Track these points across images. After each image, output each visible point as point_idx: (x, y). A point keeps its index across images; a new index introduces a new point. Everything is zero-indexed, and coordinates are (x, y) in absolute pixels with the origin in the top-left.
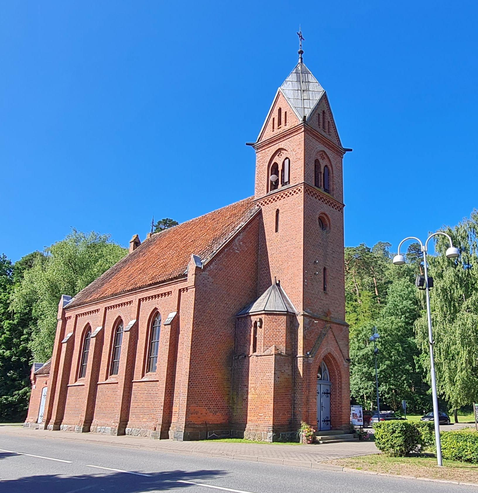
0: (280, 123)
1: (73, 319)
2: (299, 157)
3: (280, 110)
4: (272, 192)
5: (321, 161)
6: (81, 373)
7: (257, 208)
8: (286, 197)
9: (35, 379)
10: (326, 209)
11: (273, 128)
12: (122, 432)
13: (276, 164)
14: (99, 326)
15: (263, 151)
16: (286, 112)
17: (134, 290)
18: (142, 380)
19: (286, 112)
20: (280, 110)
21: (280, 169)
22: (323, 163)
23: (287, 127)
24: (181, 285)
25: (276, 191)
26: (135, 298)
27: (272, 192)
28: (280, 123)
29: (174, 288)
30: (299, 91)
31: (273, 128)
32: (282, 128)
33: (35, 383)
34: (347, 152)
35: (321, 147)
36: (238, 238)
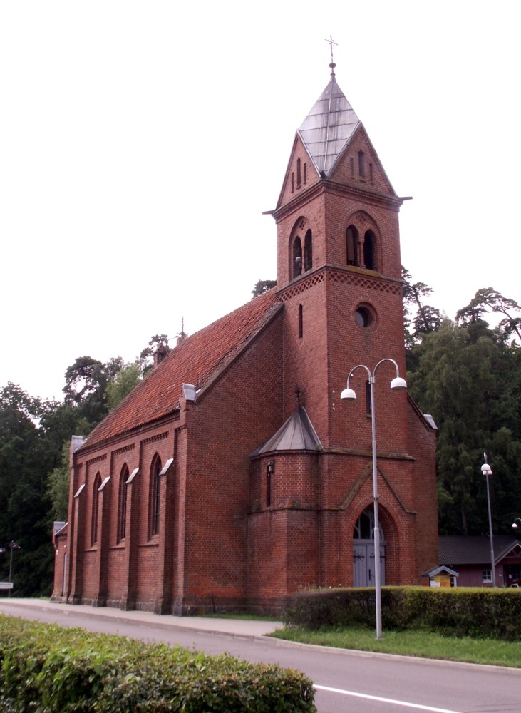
0: (299, 182)
1: (84, 469)
2: (320, 229)
3: (299, 161)
4: (295, 280)
5: (358, 226)
6: (153, 529)
7: (279, 303)
8: (317, 283)
9: (57, 542)
10: (363, 294)
11: (293, 189)
12: (132, 604)
13: (298, 239)
14: (107, 476)
15: (284, 222)
16: (305, 164)
17: (135, 430)
18: (148, 544)
19: (305, 164)
20: (299, 161)
21: (303, 244)
22: (362, 229)
23: (306, 187)
24: (176, 425)
25: (299, 277)
26: (137, 440)
27: (308, 273)
28: (299, 182)
29: (170, 427)
30: (324, 129)
31: (293, 189)
32: (303, 189)
33: (57, 546)
34: (404, 201)
35: (354, 206)
36: (248, 352)
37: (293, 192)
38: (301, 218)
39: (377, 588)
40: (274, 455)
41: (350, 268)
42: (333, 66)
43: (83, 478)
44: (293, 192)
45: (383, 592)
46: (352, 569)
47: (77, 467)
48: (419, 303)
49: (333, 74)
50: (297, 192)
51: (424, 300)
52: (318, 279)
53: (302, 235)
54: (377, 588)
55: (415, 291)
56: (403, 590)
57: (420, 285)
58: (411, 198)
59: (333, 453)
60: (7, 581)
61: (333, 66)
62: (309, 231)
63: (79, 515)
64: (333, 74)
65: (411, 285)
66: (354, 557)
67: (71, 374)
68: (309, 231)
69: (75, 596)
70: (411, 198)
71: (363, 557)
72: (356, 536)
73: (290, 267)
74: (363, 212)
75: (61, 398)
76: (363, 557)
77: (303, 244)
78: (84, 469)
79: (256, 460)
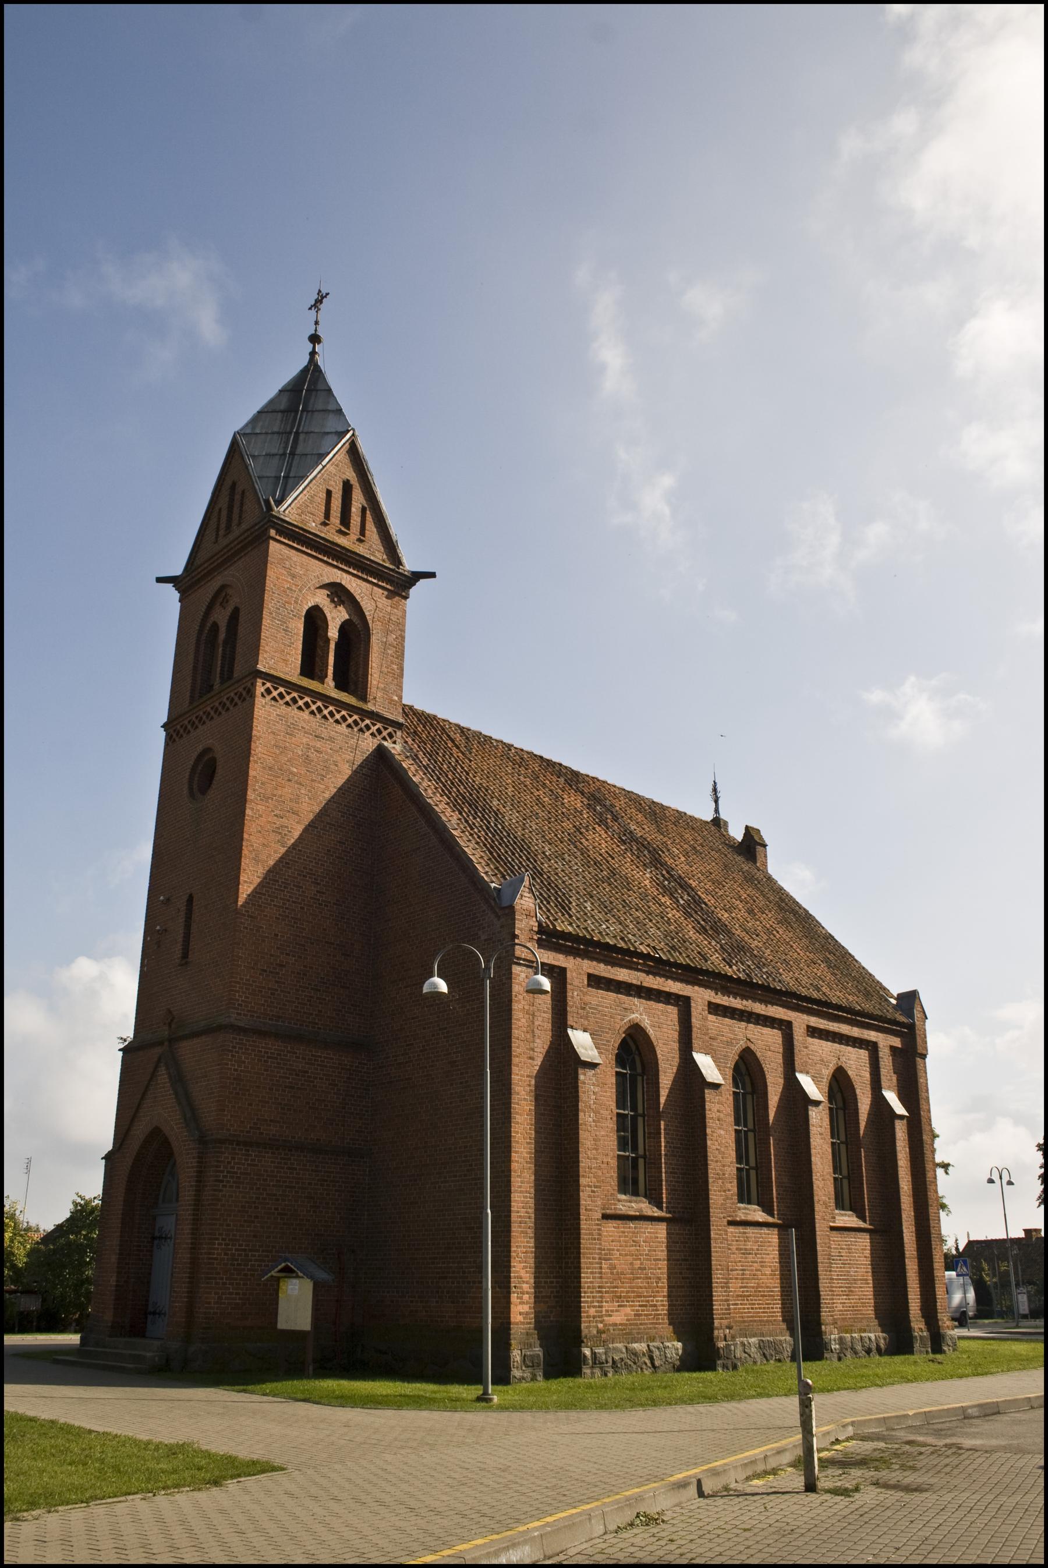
3: (234, 486)
11: (217, 535)
13: (215, 627)
20: (234, 486)
21: (222, 636)
22: (336, 617)
31: (217, 535)
37: (216, 542)
38: (223, 587)
41: (306, 682)
42: (315, 339)
44: (216, 542)
46: (1009, 1313)
49: (313, 353)
50: (223, 542)
52: (233, 699)
53: (221, 616)
58: (432, 575)
62: (236, 611)
63: (901, 1233)
64: (313, 353)
66: (154, 1238)
68: (236, 611)
70: (432, 575)
71: (170, 1238)
73: (195, 668)
74: (340, 585)
76: (170, 1238)
77: (222, 636)
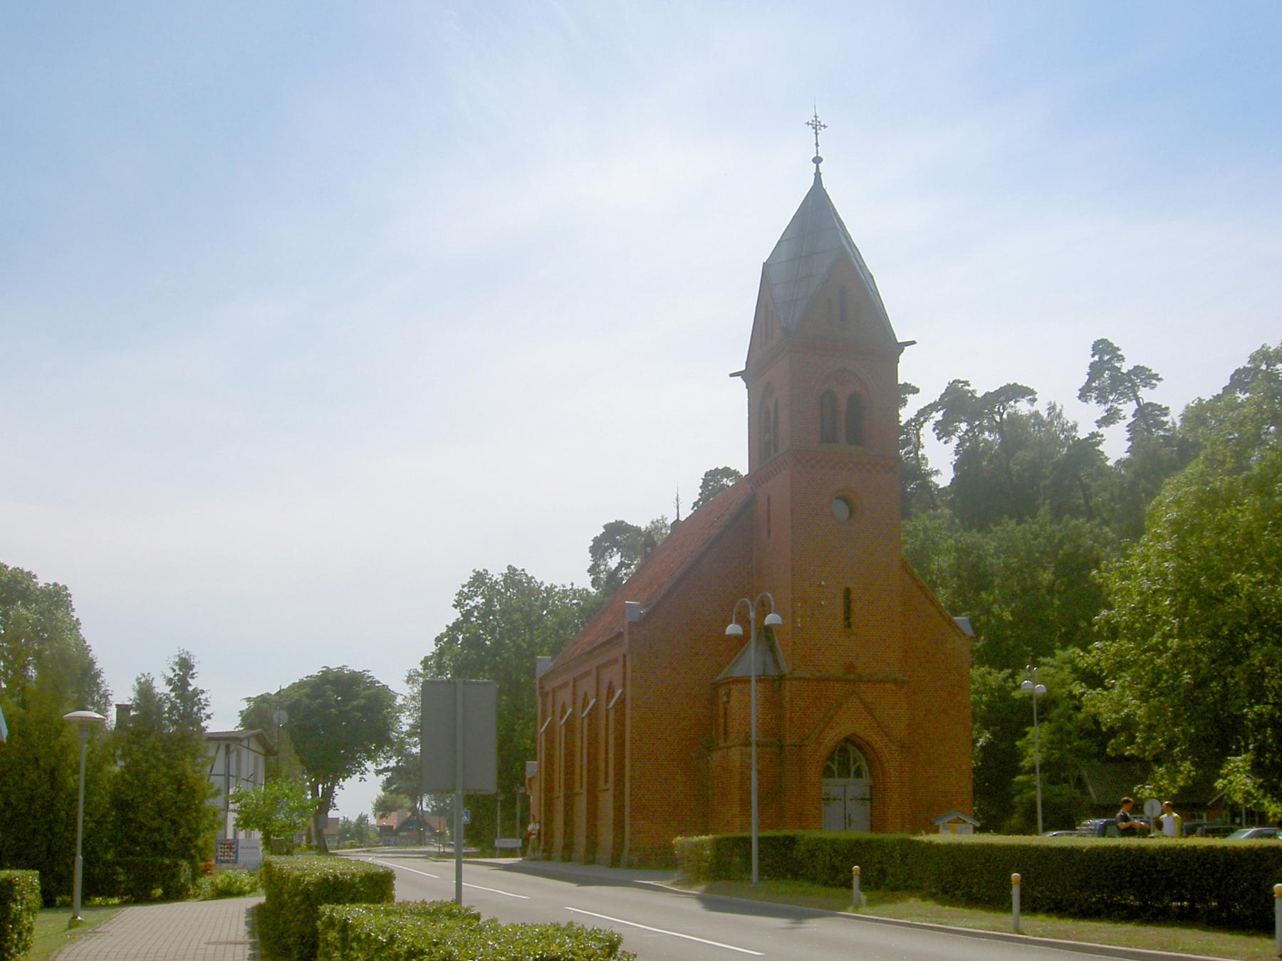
12: (591, 857)
39: (754, 834)
40: (729, 683)
43: (550, 712)
45: (762, 840)
47: (544, 695)
48: (1137, 399)
49: (818, 174)
51: (1146, 395)
54: (754, 834)
55: (1131, 381)
56: (976, 830)
57: (1139, 370)
58: (914, 343)
59: (796, 679)
60: (514, 837)
61: (817, 160)
64: (818, 174)
65: (1124, 370)
67: (599, 549)
69: (544, 850)
70: (914, 343)
72: (828, 772)
75: (584, 582)
78: (550, 696)
79: (715, 687)
